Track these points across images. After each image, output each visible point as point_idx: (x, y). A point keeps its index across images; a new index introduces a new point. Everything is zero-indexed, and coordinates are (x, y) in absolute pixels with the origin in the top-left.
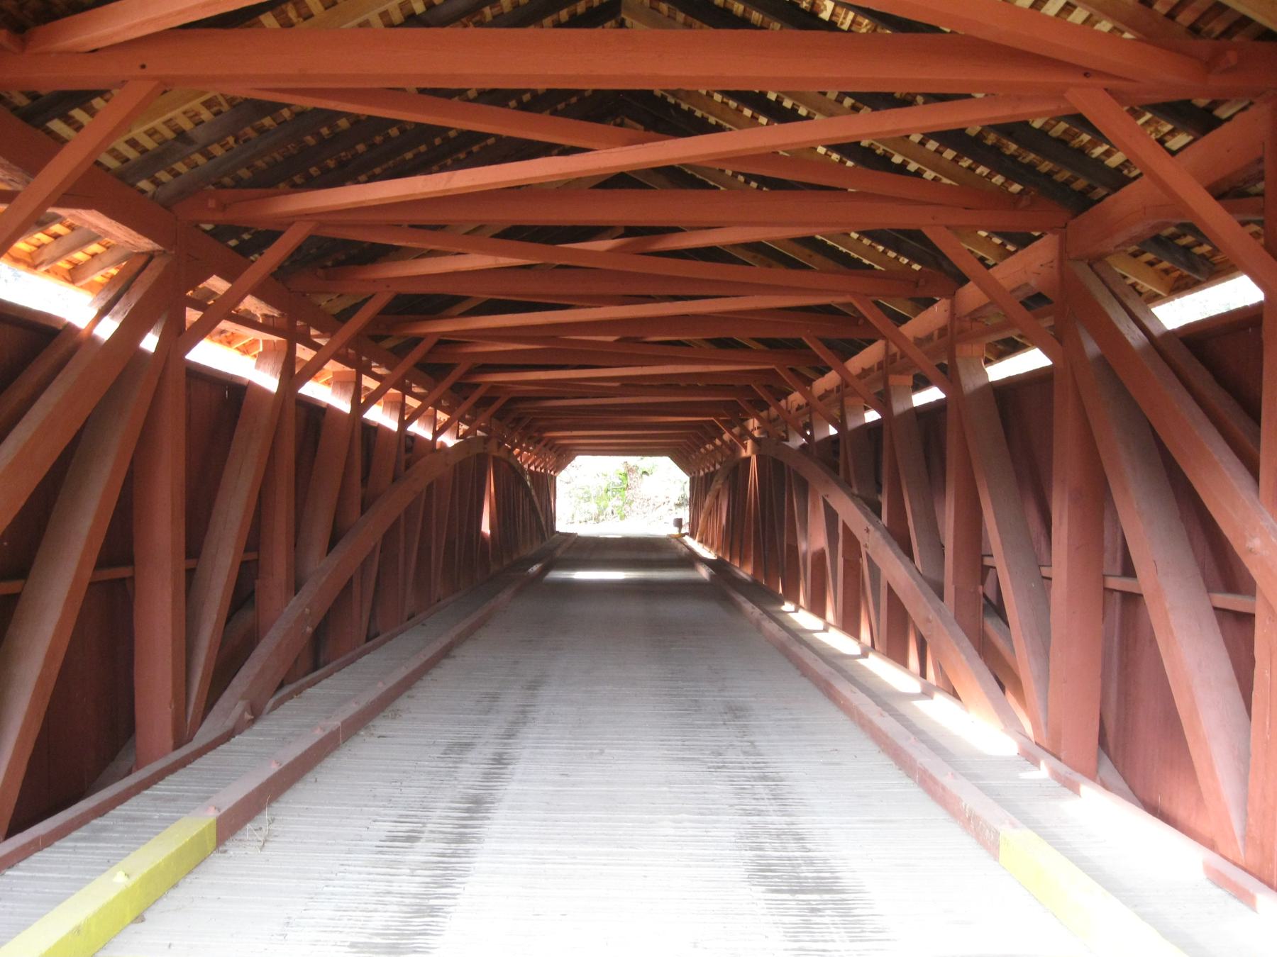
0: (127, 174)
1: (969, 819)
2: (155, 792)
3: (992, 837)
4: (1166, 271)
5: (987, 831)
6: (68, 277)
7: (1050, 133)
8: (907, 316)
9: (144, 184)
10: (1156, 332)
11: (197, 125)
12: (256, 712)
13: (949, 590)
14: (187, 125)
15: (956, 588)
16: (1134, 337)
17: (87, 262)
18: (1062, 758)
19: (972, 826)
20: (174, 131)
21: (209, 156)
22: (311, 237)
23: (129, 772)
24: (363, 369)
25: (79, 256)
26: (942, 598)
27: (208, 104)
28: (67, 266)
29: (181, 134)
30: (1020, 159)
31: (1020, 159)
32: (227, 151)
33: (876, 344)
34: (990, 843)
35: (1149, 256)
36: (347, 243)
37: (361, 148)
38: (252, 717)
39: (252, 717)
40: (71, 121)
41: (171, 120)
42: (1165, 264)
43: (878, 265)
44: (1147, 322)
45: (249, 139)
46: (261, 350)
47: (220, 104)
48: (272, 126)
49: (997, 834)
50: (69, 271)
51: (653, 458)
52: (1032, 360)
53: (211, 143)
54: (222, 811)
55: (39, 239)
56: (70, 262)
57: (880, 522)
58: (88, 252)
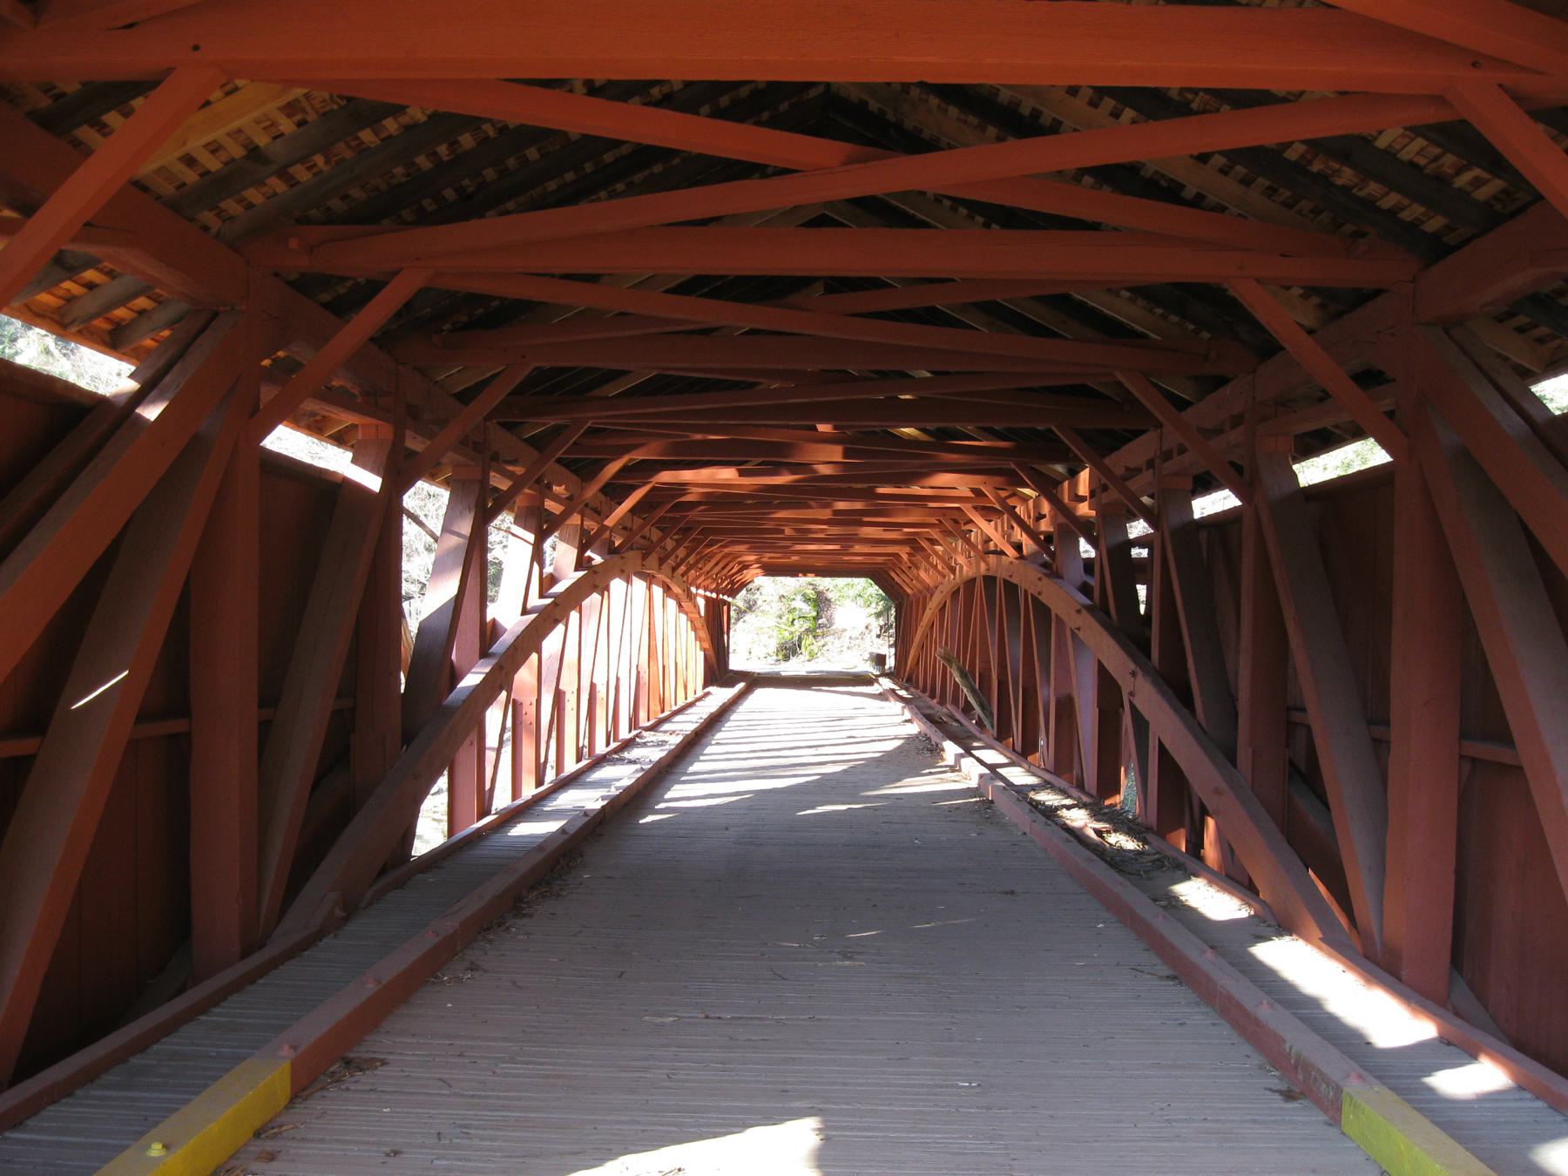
0: (183, 204)
1: (1296, 1067)
2: (215, 1018)
3: (1331, 1092)
4: (1541, 340)
5: (1324, 1086)
6: (108, 339)
7: (1398, 156)
8: (1188, 401)
9: (207, 217)
10: (1538, 417)
11: (275, 138)
12: (351, 908)
13: (1244, 754)
14: (262, 140)
15: (1254, 751)
16: (1510, 422)
17: (133, 321)
18: (1404, 978)
19: (1300, 1077)
20: (245, 147)
21: (291, 181)
22: (423, 291)
23: (181, 990)
24: (495, 460)
25: (121, 313)
26: (1234, 763)
27: (290, 109)
28: (107, 326)
29: (254, 152)
30: (1354, 191)
31: (1354, 191)
32: (314, 175)
33: (1144, 437)
34: (1328, 1101)
35: (1522, 320)
36: (473, 299)
37: (489, 174)
38: (344, 914)
39: (344, 914)
40: (107, 130)
41: (240, 131)
42: (1543, 330)
43: (1153, 332)
44: (1527, 406)
45: (344, 160)
46: (360, 438)
47: (303, 110)
48: (372, 143)
49: (1339, 1090)
50: (111, 333)
51: (1328, 479)
52: (1365, 455)
53: (293, 164)
54: (300, 1050)
55: (69, 291)
56: (108, 320)
57: (1149, 663)
58: (135, 308)
